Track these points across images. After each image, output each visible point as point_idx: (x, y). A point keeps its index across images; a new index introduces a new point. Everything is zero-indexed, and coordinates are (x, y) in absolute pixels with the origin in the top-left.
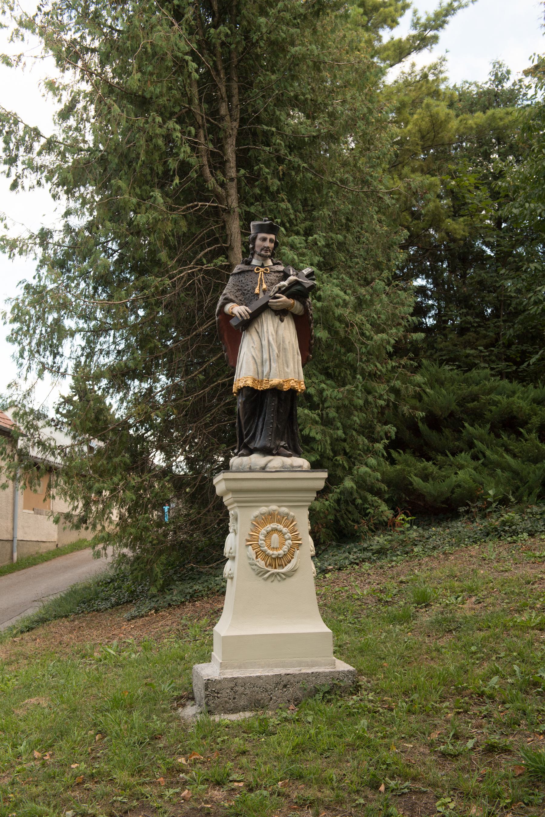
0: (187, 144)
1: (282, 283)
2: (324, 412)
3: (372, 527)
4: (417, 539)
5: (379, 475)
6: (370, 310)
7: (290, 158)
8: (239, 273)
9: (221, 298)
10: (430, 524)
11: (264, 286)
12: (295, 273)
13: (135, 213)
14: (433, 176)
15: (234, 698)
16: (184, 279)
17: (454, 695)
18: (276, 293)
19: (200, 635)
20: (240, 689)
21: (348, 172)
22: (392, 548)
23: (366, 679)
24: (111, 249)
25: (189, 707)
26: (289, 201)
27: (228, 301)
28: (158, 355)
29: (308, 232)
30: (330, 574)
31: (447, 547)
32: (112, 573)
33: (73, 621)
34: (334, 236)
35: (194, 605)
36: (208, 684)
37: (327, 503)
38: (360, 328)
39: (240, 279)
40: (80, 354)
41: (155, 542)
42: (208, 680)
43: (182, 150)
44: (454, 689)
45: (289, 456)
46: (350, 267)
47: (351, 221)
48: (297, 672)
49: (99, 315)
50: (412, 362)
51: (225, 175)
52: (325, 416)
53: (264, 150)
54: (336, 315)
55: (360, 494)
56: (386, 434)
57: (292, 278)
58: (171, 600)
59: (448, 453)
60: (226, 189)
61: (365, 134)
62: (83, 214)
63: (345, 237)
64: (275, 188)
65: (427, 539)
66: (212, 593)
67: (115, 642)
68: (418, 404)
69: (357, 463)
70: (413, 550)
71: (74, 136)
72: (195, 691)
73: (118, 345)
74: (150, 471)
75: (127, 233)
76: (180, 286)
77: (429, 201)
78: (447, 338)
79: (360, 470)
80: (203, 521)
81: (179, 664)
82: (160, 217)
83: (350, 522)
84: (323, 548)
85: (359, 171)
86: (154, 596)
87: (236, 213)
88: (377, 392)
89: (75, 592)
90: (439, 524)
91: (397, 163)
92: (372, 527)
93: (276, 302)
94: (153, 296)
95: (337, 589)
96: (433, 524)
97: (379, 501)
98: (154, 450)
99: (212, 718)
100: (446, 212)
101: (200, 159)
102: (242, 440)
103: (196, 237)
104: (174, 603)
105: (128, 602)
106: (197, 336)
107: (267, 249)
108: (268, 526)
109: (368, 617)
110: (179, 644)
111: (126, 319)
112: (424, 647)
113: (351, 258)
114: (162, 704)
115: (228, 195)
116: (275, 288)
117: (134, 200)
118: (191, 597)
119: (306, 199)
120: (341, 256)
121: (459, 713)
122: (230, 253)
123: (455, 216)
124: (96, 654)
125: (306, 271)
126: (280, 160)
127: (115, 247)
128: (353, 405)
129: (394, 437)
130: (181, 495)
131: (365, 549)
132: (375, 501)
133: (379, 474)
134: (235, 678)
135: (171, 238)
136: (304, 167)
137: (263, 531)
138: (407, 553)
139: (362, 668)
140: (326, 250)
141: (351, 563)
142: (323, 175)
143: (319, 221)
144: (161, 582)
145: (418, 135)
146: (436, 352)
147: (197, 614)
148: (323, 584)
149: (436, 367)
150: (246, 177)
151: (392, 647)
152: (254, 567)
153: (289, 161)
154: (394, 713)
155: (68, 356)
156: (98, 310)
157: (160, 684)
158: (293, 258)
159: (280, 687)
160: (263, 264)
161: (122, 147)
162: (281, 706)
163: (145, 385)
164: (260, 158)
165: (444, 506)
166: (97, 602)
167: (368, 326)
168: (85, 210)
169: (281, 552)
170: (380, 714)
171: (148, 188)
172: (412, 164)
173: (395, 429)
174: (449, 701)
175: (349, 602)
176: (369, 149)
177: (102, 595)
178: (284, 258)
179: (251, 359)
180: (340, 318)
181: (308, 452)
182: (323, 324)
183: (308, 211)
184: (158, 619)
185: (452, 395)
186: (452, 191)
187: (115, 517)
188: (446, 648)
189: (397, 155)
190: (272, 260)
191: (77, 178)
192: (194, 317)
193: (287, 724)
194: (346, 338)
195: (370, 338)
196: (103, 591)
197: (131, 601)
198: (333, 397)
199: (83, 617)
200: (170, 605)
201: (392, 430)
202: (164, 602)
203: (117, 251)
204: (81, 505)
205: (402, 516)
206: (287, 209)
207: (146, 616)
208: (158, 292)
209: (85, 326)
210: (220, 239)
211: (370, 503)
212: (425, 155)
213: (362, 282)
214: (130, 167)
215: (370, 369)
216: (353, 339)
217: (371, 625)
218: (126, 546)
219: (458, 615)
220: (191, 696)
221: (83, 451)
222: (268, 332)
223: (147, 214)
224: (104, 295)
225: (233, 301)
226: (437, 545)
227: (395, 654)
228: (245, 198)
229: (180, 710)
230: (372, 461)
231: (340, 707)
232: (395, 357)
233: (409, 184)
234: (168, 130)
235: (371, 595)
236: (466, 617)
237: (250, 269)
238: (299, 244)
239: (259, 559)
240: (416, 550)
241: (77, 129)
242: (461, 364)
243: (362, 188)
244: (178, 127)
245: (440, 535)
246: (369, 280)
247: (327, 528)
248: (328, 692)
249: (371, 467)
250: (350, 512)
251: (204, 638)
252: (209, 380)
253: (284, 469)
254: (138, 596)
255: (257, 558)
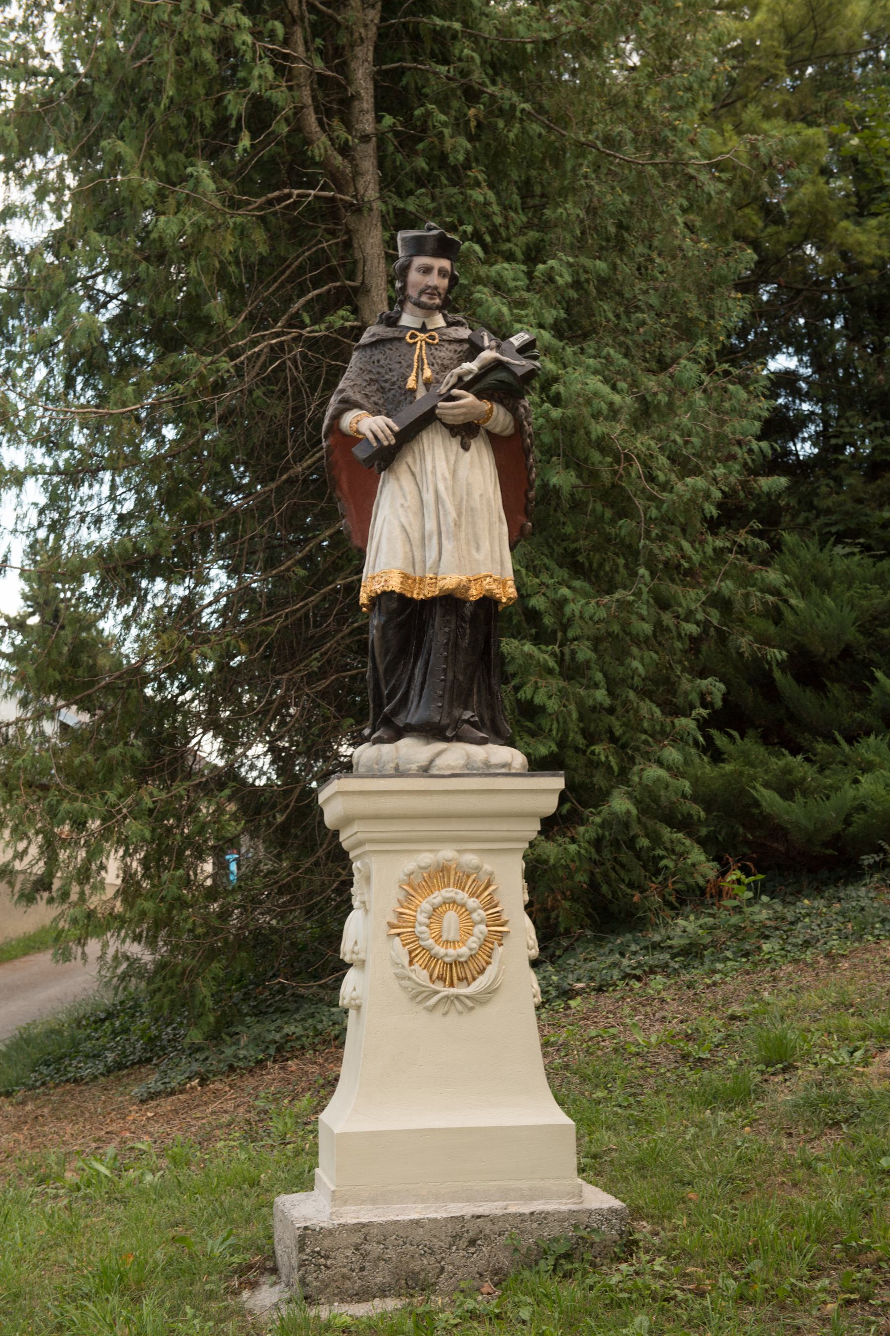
0: (266, 60)
1: (467, 366)
2: (566, 650)
3: (672, 899)
4: (768, 923)
5: (686, 785)
6: (668, 427)
7: (491, 89)
8: (373, 345)
9: (334, 400)
10: (799, 892)
11: (428, 373)
12: (493, 343)
13: (158, 214)
14: (810, 124)
15: (362, 1269)
16: (262, 358)
17: (840, 1262)
18: (453, 387)
19: (295, 1132)
20: (375, 1249)
21: (621, 121)
22: (714, 944)
23: (649, 1227)
24: (104, 292)
25: (265, 1288)
26: (491, 186)
27: (348, 404)
28: (206, 524)
29: (533, 254)
30: (579, 999)
31: (835, 942)
32: (108, 999)
33: (23, 1103)
34: (587, 262)
35: (283, 1068)
36: (305, 1236)
37: (573, 848)
38: (645, 465)
39: (375, 358)
40: (34, 523)
41: (199, 931)
42: (306, 1228)
43: (256, 73)
44: (842, 1251)
45: (482, 742)
46: (626, 331)
47: (627, 229)
48: (500, 1212)
49: (78, 437)
50: (757, 540)
51: (349, 127)
52: (567, 657)
53: (435, 73)
54: (594, 437)
55: (645, 827)
56: (702, 696)
57: (487, 355)
58: (236, 1056)
59: (839, 738)
60: (352, 160)
61: (660, 35)
62: (42, 215)
63: (614, 267)
64: (461, 157)
65: (792, 923)
66: (325, 1041)
67: (110, 1150)
68: (772, 630)
69: (638, 759)
70: (759, 948)
71: (20, 42)
72: (279, 1252)
73: (120, 502)
74: (189, 775)
75: (137, 257)
76: (253, 374)
77: (800, 183)
78: (841, 486)
79: (645, 774)
80: (304, 886)
81: (246, 1195)
82: (209, 222)
83: (623, 887)
84: (565, 943)
85: (647, 119)
86: (199, 1049)
87: (376, 214)
88: (680, 605)
89: (28, 1041)
90: (819, 892)
91: (733, 98)
92: (672, 899)
93: (453, 408)
94: (194, 395)
95: (594, 1033)
96: (805, 892)
97: (688, 842)
98: (200, 731)
99: (312, 1313)
100: (839, 206)
101: (296, 93)
102: (379, 706)
103: (288, 267)
104: (241, 1064)
105: (142, 1062)
106: (290, 481)
107: (433, 291)
108: (436, 893)
109: (657, 1092)
110: (248, 1152)
111: (138, 447)
112: (778, 1157)
113: (628, 313)
114: (207, 1282)
115: (357, 173)
116: (450, 378)
117: (151, 184)
118: (279, 1050)
119: (528, 182)
120: (606, 309)
121: (849, 1303)
122: (362, 302)
123: (861, 215)
124: (68, 1175)
125: (517, 340)
126: (472, 95)
127: (111, 287)
128: (630, 634)
129: (719, 704)
130: (257, 828)
131: (656, 946)
132: (679, 841)
133: (687, 784)
134: (364, 1225)
135: (232, 269)
136: (523, 110)
137: (426, 905)
138: (747, 954)
139: (641, 1202)
140: (573, 294)
141: (626, 976)
142: (565, 128)
143: (559, 230)
144: (212, 1019)
145: (780, 35)
146: (817, 517)
147: (291, 1087)
148: (564, 1021)
149: (814, 546)
150: (397, 134)
151: (708, 1158)
152: (406, 983)
153: (492, 96)
154: (707, 1302)
155: (11, 527)
156: (76, 428)
157: (203, 1239)
158: (500, 311)
159: (463, 1244)
160: (424, 324)
161: (123, 67)
162: (463, 1285)
163: (179, 592)
164: (427, 90)
165: (829, 851)
166: (74, 1063)
167: (663, 460)
168: (46, 207)
169: (464, 951)
170: (678, 1304)
171: (181, 157)
172: (764, 101)
173: (722, 686)
174: (829, 1276)
175: (617, 1061)
176: (668, 69)
177: (87, 1046)
178: (479, 311)
179: (397, 532)
180: (603, 445)
181: (533, 734)
182: (565, 455)
183: (535, 206)
184: (205, 1099)
185: (847, 609)
186: (855, 160)
187: (112, 876)
188: (826, 1161)
189: (732, 82)
190: (445, 316)
191: (25, 137)
192: (284, 442)
193: (475, 1325)
194: (614, 486)
195: (666, 487)
196: (89, 1038)
197: (149, 1060)
198: (587, 616)
199: (45, 1094)
200: (232, 1068)
201: (715, 688)
202: (219, 1061)
203: (115, 297)
204: (34, 851)
205: (735, 875)
206: (487, 203)
207: (181, 1092)
208: (206, 388)
209: (49, 462)
210: (340, 271)
211: (668, 845)
212: (795, 79)
213: (654, 365)
214: (141, 111)
215: (667, 554)
216: (630, 489)
217: (665, 1111)
218: (137, 938)
219: (854, 1089)
220: (269, 1264)
221: (42, 733)
222: (434, 473)
223: (180, 215)
224: (90, 393)
225: (360, 407)
226: (814, 937)
227: (714, 1174)
228: (394, 179)
229: (246, 1294)
230: (672, 754)
231: (591, 1288)
232: (723, 529)
233: (754, 147)
234: (225, 27)
235: (666, 1046)
236: (872, 1094)
237: (396, 334)
238: (514, 280)
239: (416, 966)
240: (766, 947)
241: (25, 27)
242: (873, 543)
243: (652, 157)
244: (246, 21)
245: (820, 914)
246: (668, 360)
247: (574, 899)
248: (568, 1256)
249: (669, 769)
250: (623, 866)
251: (304, 1138)
252: (319, 579)
253: (469, 771)
254: (163, 1048)
255: (411, 963)
